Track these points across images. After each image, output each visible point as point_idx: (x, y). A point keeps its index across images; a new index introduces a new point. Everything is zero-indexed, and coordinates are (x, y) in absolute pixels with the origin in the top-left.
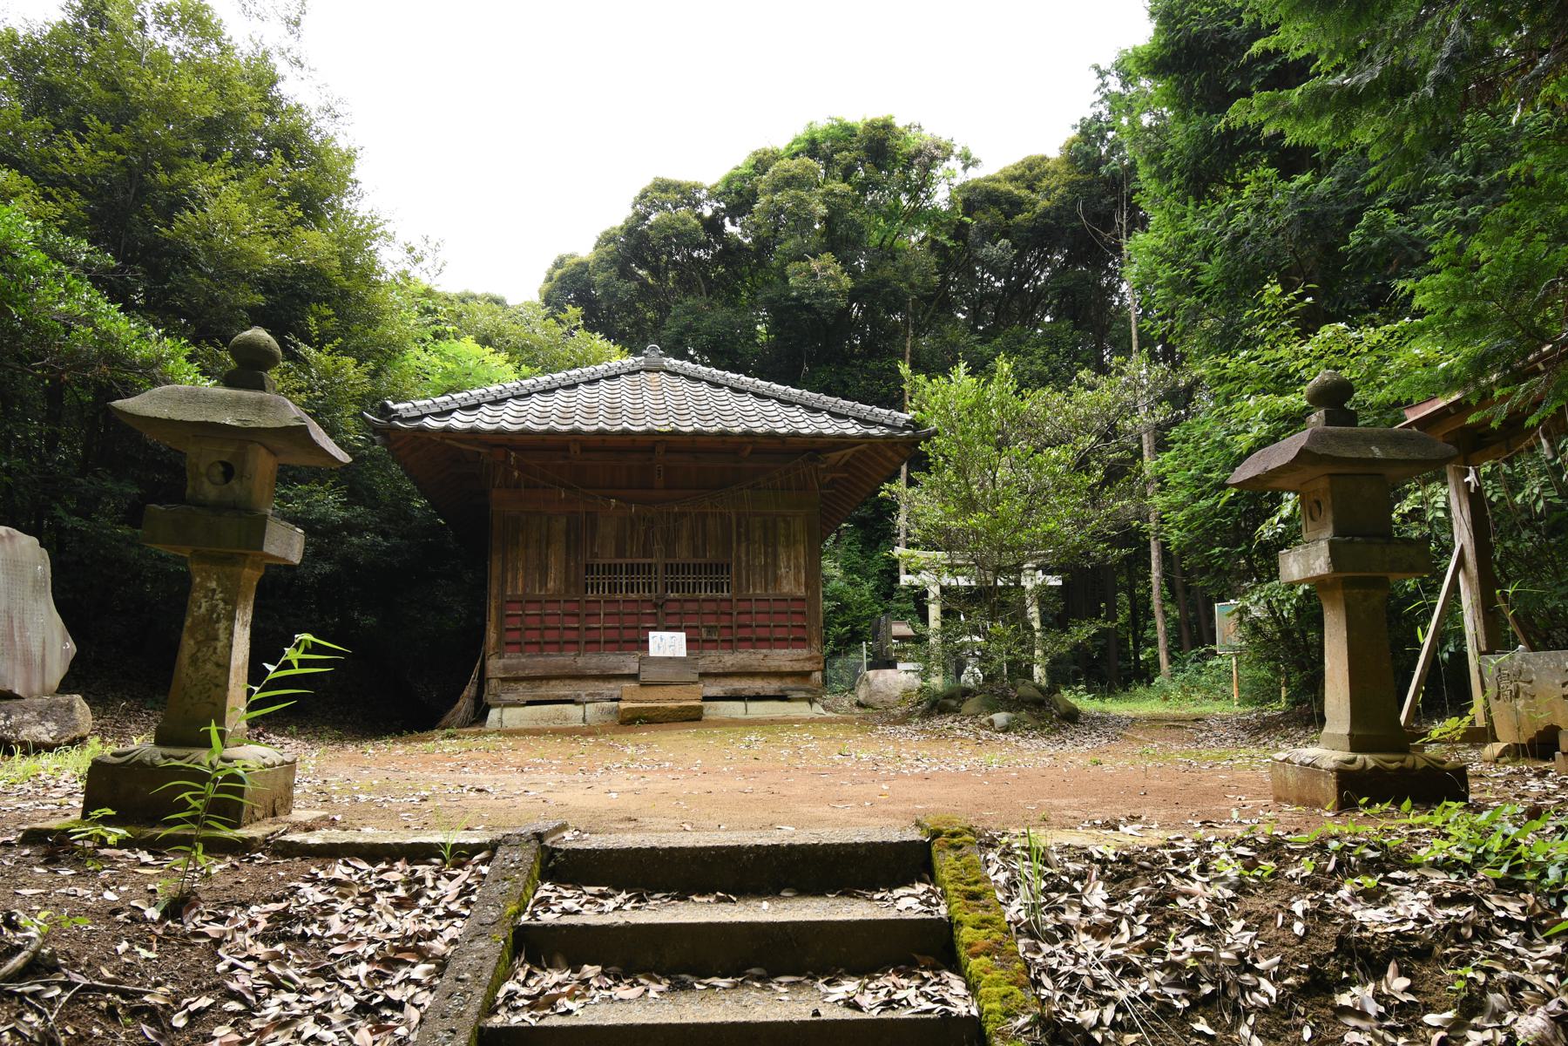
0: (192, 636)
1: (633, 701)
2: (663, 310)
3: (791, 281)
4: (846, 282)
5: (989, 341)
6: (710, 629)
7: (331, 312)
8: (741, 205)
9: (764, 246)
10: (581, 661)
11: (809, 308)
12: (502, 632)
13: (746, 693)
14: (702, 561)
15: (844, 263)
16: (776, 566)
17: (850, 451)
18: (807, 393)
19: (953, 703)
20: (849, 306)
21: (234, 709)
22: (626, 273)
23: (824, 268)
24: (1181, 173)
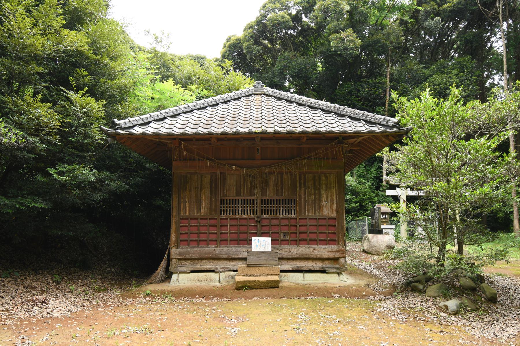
1: (244, 275)
2: (274, 58)
3: (332, 44)
4: (359, 42)
5: (429, 67)
6: (285, 234)
7: (86, 73)
8: (309, 7)
9: (320, 27)
10: (218, 250)
11: (340, 55)
12: (178, 234)
13: (304, 269)
14: (281, 198)
15: (358, 33)
16: (320, 200)
18: (337, 106)
19: (421, 287)
20: (361, 53)
21: (235, 118)
22: (257, 42)
23: (348, 36)
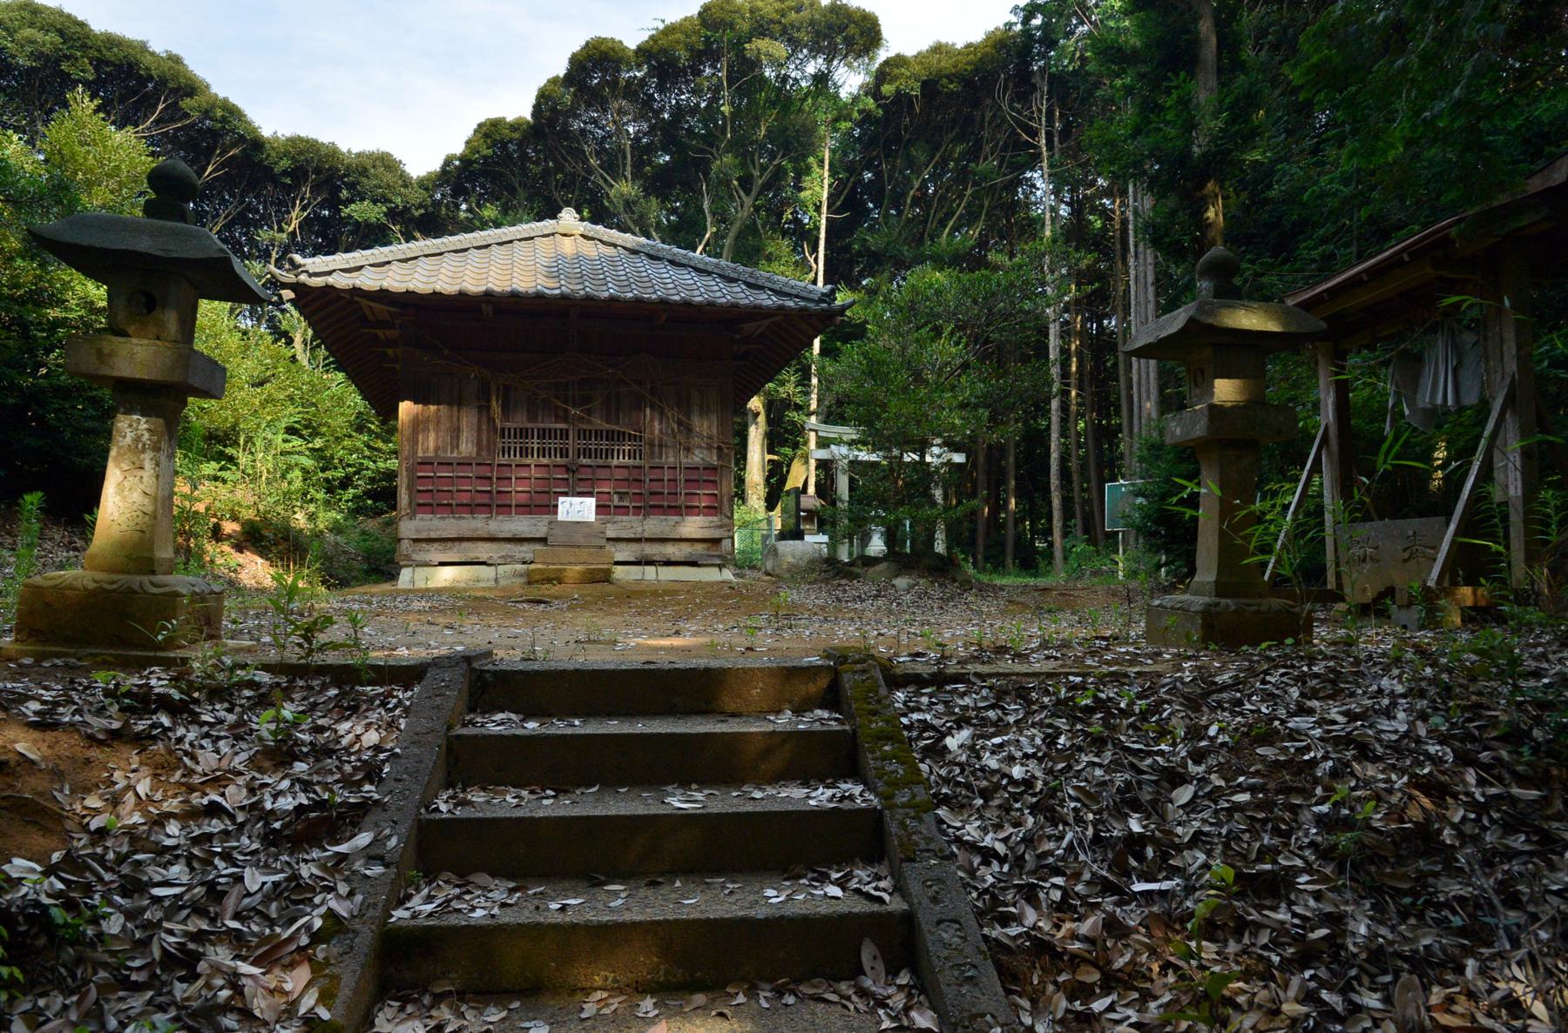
0: (118, 466)
17: (766, 322)
24: (1359, 842)
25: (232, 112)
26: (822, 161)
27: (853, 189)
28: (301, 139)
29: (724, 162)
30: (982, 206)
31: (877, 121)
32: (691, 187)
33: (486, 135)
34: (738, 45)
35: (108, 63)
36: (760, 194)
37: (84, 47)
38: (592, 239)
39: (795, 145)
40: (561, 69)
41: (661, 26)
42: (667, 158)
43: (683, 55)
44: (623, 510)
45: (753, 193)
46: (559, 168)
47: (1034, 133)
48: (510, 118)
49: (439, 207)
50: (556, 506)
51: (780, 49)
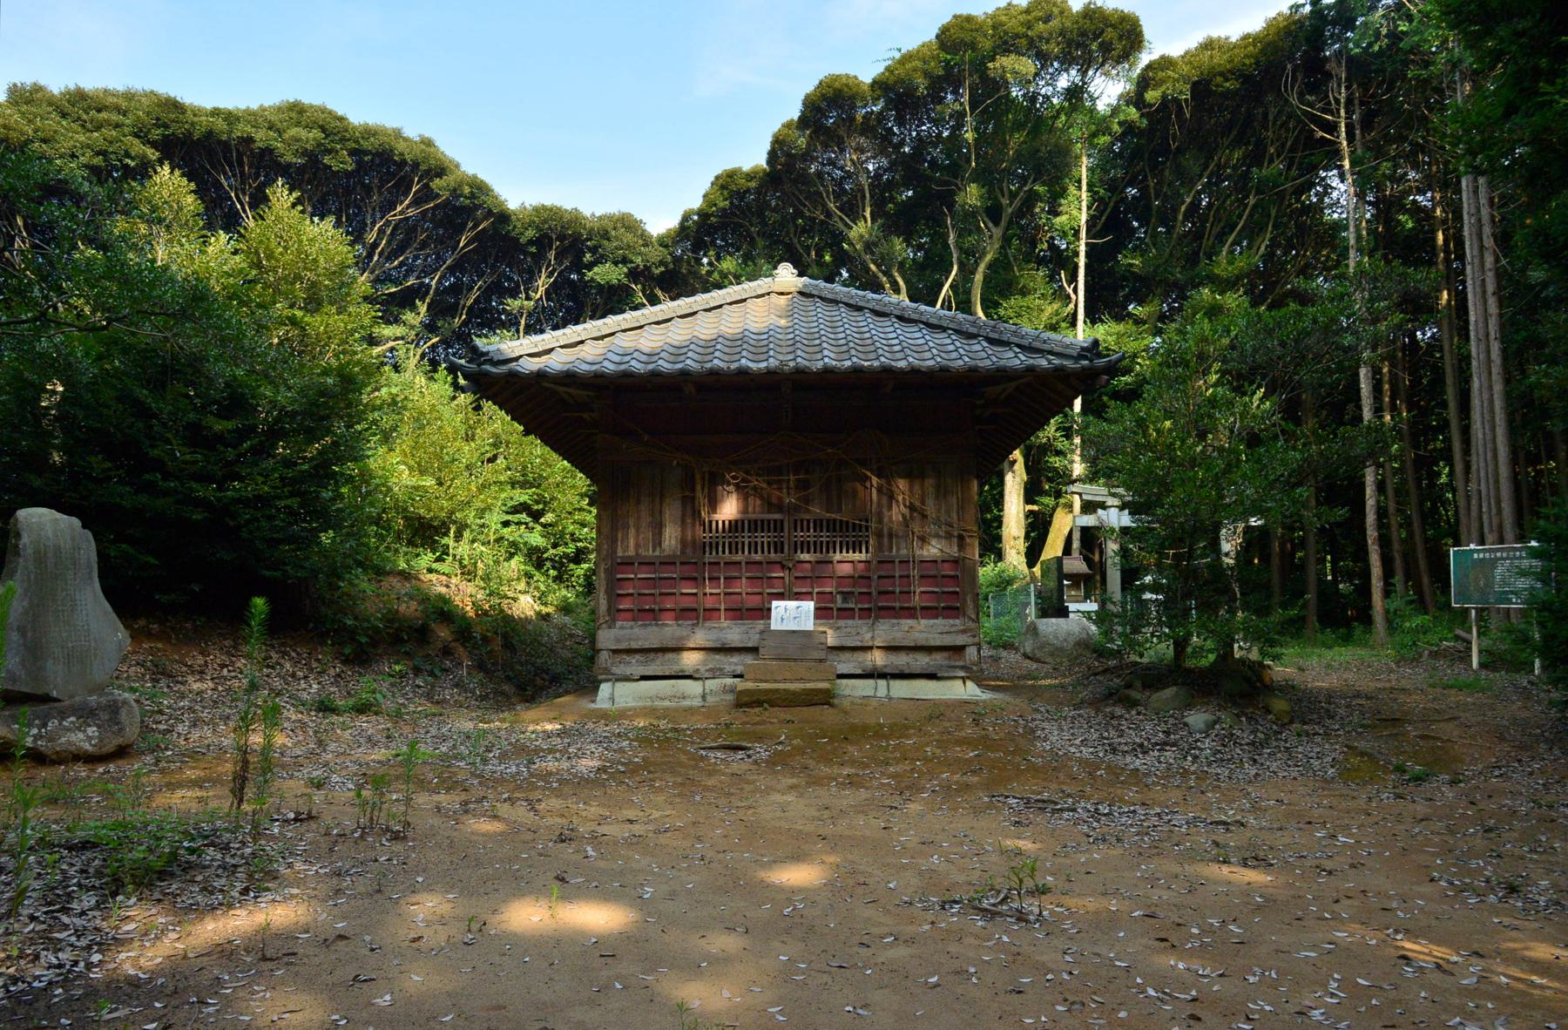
17: (1014, 384)
25: (480, 188)
26: (1079, 181)
27: (1116, 207)
28: (544, 208)
29: (972, 195)
30: (1269, 216)
31: (1141, 133)
32: (937, 222)
33: (723, 187)
34: (980, 67)
35: (366, 152)
36: (1010, 223)
37: (343, 140)
38: (812, 296)
39: (1051, 170)
40: (795, 113)
41: (897, 55)
42: (910, 193)
43: (922, 85)
44: (845, 613)
45: (1003, 223)
46: (798, 214)
47: (1332, 128)
48: (746, 167)
49: (677, 269)
50: (770, 610)
51: (1027, 65)
